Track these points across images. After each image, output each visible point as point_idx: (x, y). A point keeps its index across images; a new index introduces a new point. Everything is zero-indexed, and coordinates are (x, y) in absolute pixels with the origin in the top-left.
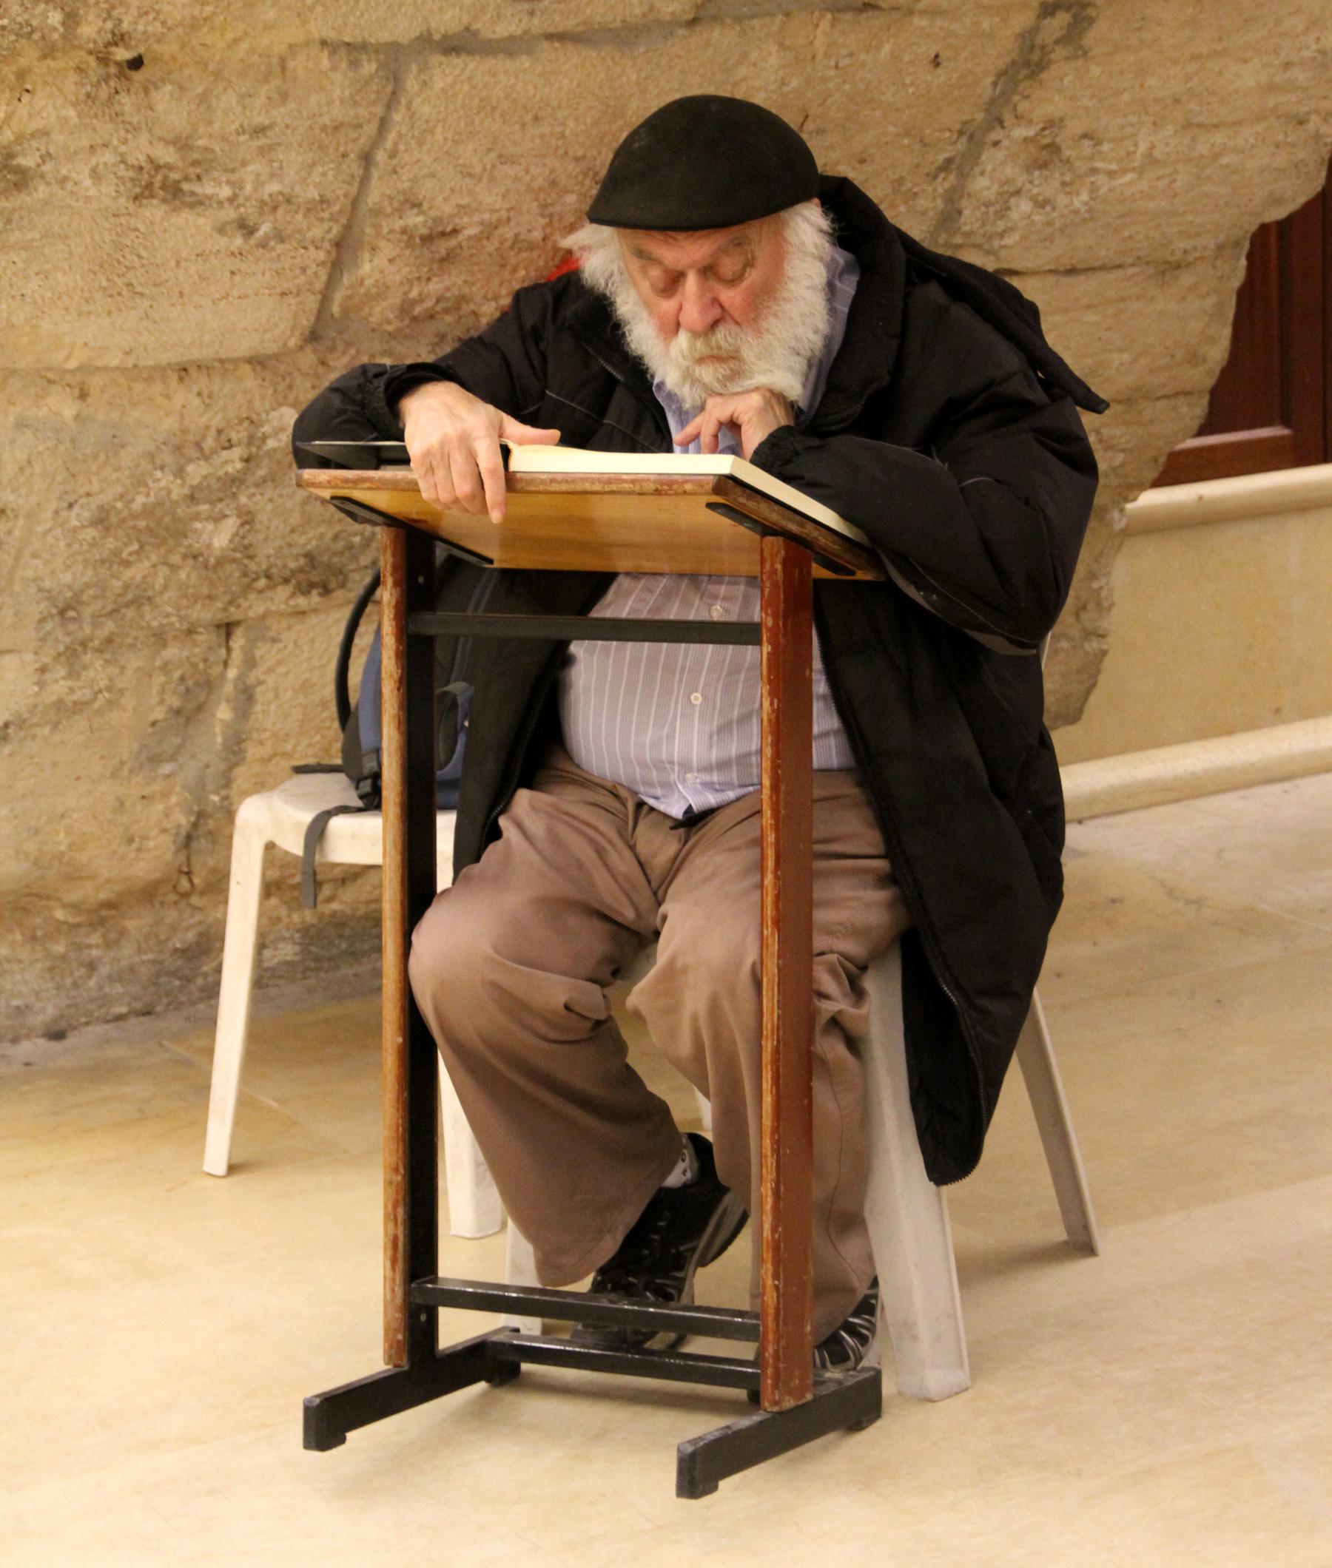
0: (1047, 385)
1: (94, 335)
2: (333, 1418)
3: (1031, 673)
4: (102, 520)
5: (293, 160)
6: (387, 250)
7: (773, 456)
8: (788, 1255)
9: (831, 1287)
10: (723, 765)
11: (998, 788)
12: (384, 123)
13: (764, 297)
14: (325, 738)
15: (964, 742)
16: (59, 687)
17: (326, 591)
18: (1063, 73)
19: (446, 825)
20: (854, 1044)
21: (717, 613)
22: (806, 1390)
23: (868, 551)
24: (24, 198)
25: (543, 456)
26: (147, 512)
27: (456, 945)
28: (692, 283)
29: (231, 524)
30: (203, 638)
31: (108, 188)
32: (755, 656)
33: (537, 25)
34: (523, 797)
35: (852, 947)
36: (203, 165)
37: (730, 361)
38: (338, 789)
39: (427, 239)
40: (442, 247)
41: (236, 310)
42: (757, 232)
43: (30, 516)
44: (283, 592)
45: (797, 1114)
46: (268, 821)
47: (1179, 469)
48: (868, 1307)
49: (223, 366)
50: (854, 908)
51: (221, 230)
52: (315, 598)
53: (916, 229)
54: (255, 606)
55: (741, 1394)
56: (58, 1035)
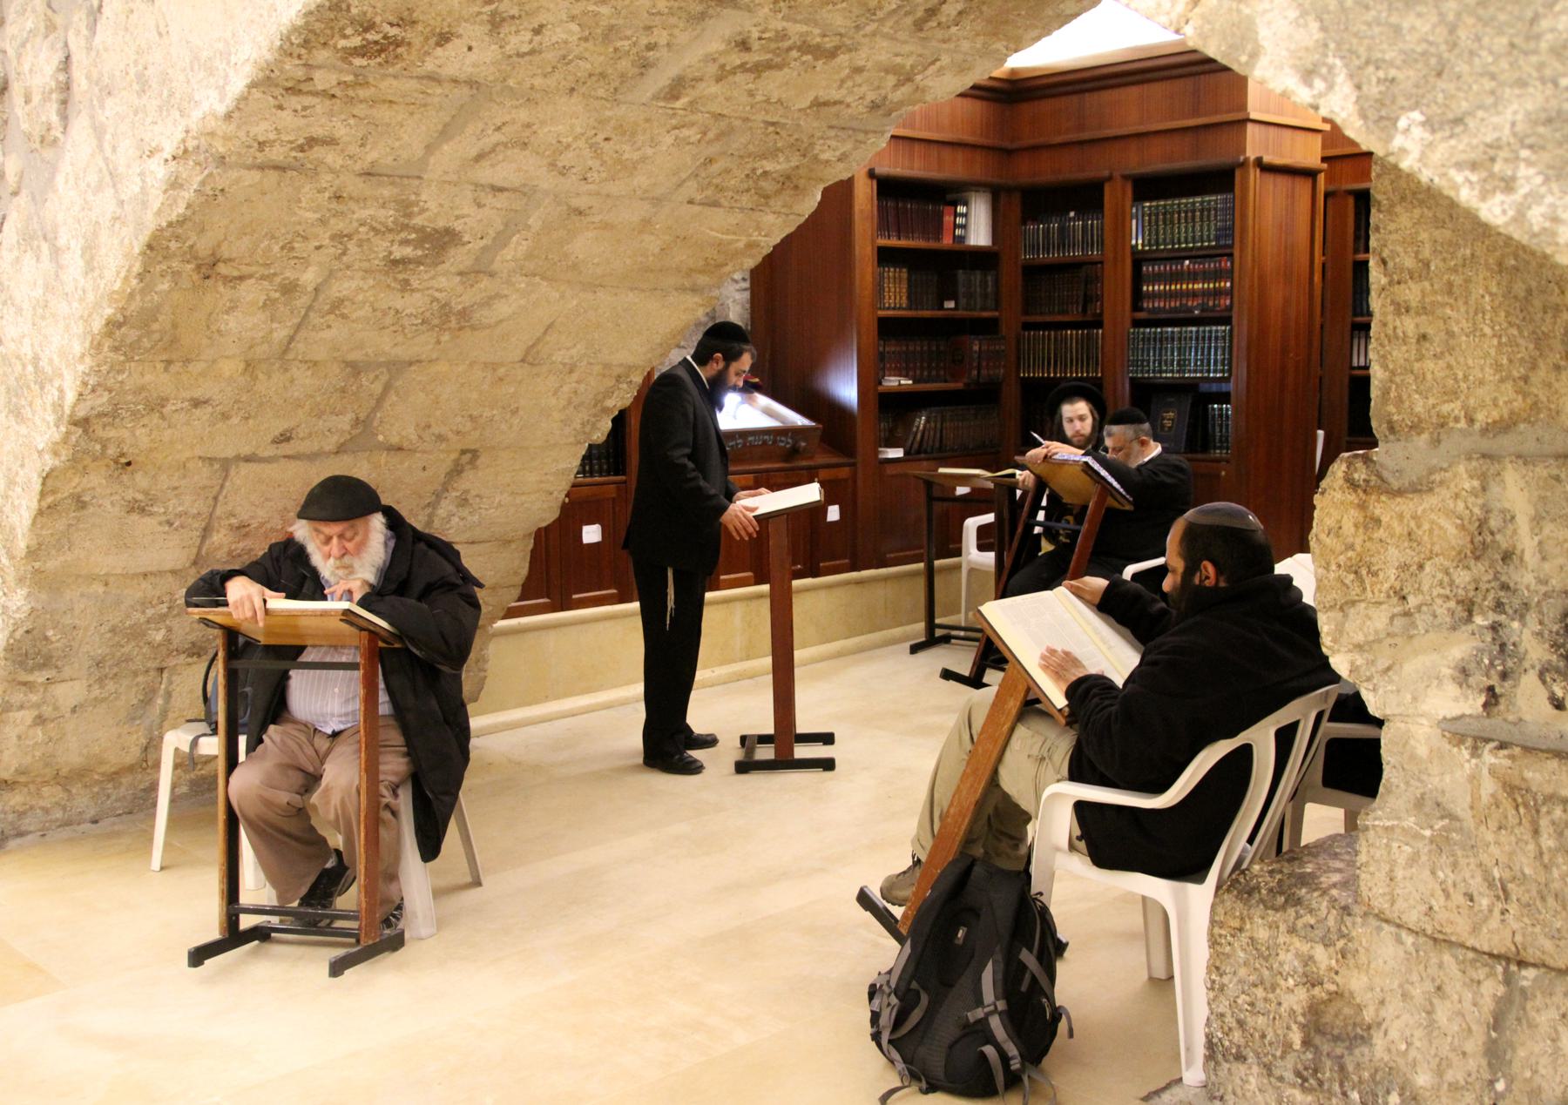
0: (463, 579)
1: (111, 562)
2: (199, 956)
3: (457, 679)
4: (113, 630)
5: (188, 499)
6: (223, 531)
7: (363, 603)
8: (370, 890)
9: (386, 901)
10: (346, 714)
11: (447, 722)
12: (222, 487)
14: (199, 709)
15: (434, 703)
16: (96, 692)
17: (199, 656)
18: (469, 474)
19: (242, 741)
20: (394, 813)
21: (344, 659)
22: (381, 936)
23: (399, 638)
24: (86, 512)
25: (279, 602)
26: (131, 627)
27: (247, 782)
28: (335, 540)
29: (163, 632)
30: (152, 673)
31: (117, 509)
32: (358, 675)
33: (279, 452)
34: (272, 728)
35: (394, 779)
36: (153, 500)
37: (350, 569)
38: (203, 727)
39: (238, 528)
40: (244, 531)
41: (168, 554)
42: (359, 523)
43: (86, 629)
44: (183, 657)
45: (373, 841)
46: (176, 740)
47: (511, 613)
48: (400, 907)
49: (160, 573)
50: (394, 765)
51: (160, 524)
52: (195, 658)
53: (419, 527)
54: (171, 662)
55: (353, 940)
56: (95, 822)
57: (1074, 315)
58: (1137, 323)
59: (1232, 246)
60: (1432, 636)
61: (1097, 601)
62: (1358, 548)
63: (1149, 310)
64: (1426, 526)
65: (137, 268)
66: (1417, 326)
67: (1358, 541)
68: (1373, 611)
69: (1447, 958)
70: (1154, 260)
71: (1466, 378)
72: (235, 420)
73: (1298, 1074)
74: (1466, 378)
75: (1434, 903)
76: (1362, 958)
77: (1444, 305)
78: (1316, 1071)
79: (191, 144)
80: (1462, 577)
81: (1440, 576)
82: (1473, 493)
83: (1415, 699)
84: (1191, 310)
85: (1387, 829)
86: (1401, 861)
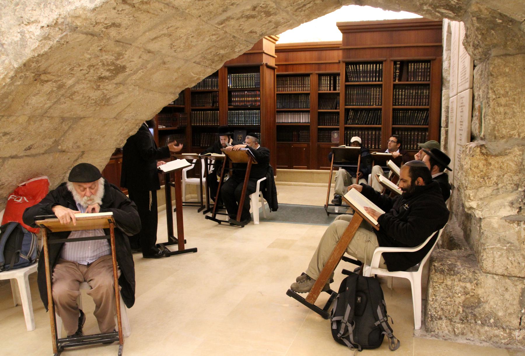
10: (94, 256)
13: (96, 191)
28: (88, 189)
33: (26, 154)
57: (209, 106)
58: (230, 109)
59: (259, 88)
60: (504, 194)
61: (361, 191)
62: (485, 171)
63: (234, 106)
64: (505, 165)
65: (12, 74)
66: (504, 110)
67: (484, 170)
68: (487, 189)
69: (507, 280)
70: (235, 91)
71: (518, 124)
72: (15, 141)
73: (461, 319)
74: (518, 124)
75: (508, 266)
76: (483, 285)
77: (512, 104)
78: (467, 318)
79: (60, 21)
80: (516, 178)
81: (509, 178)
82: (520, 155)
83: (495, 212)
84: (247, 106)
85: (492, 248)
86: (497, 256)
